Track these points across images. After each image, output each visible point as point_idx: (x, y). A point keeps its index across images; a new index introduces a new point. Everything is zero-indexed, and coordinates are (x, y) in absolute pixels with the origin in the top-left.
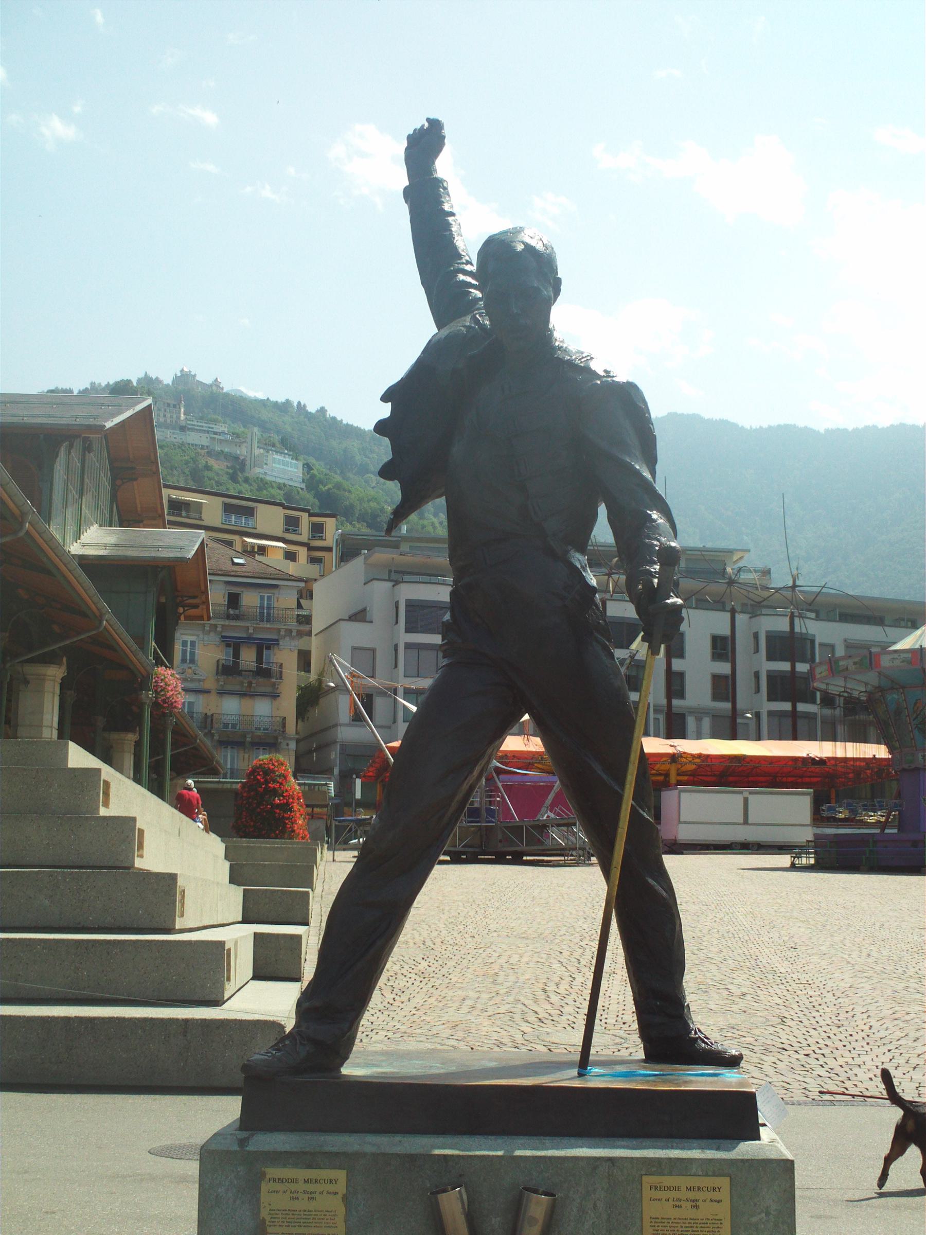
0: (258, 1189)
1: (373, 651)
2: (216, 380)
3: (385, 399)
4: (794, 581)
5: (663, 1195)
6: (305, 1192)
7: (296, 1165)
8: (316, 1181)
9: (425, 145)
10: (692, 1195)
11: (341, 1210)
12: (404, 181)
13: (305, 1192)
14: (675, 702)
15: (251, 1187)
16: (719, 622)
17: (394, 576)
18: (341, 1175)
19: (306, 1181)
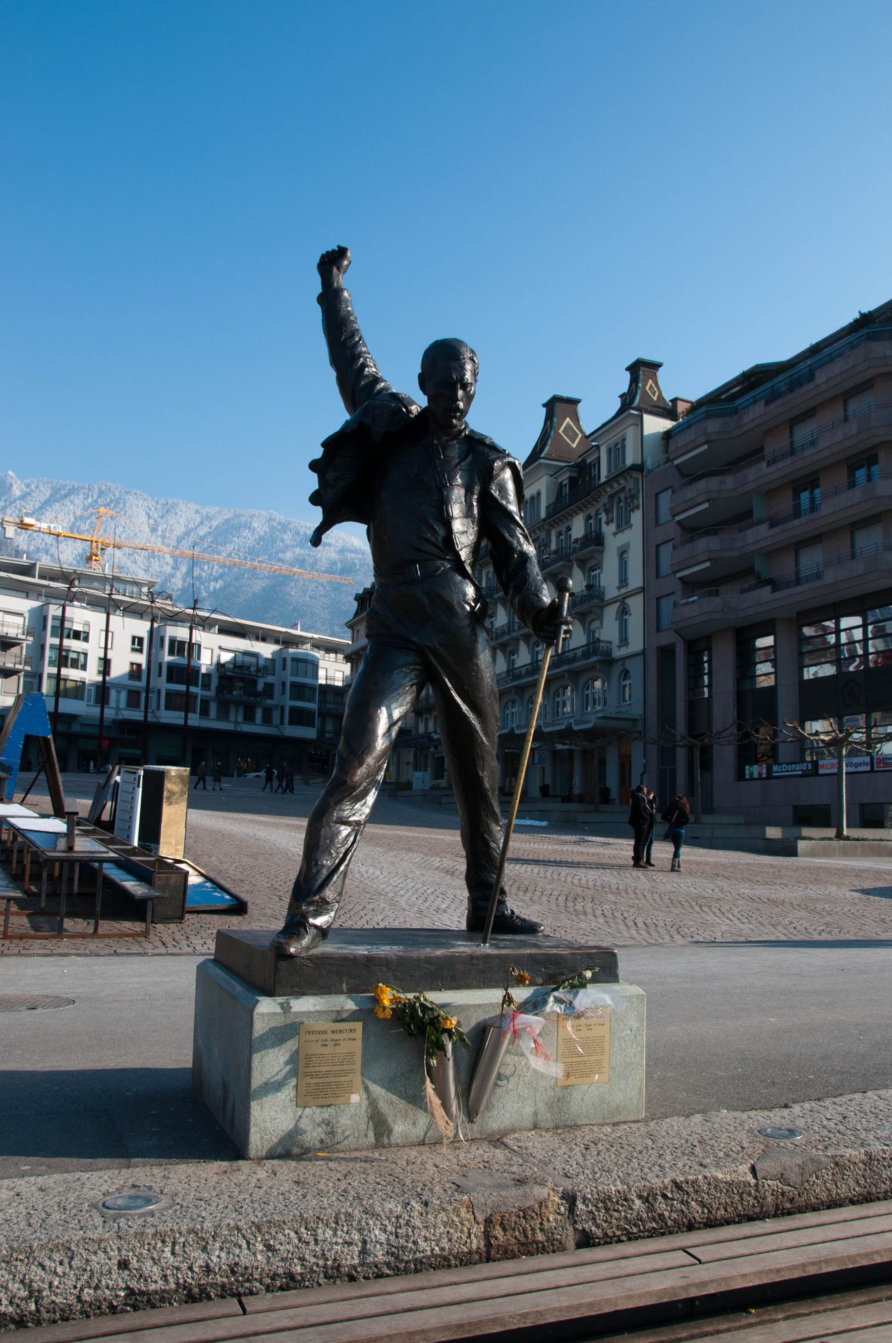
3: (323, 445)
6: (332, 1040)
8: (340, 1031)
9: (331, 261)
12: (319, 290)
13: (332, 1040)
19: (333, 1032)
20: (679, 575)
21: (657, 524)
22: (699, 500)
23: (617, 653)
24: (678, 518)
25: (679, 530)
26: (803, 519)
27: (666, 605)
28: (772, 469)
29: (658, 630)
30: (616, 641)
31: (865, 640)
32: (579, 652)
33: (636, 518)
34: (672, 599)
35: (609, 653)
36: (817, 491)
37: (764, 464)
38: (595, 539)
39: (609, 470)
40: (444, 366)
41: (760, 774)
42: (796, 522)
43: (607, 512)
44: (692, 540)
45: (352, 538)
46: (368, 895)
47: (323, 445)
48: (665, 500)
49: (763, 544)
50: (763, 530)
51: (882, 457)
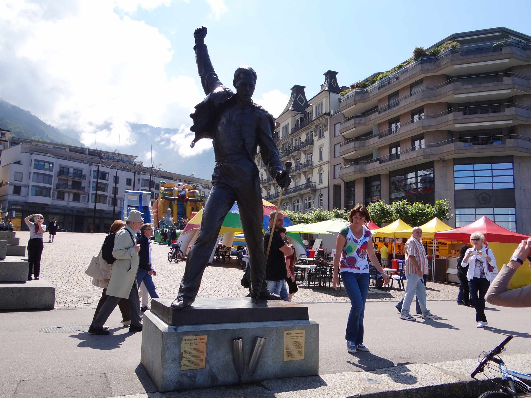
0: (181, 343)
1: (22, 173)
2: (338, 73)
3: (195, 108)
5: (289, 336)
7: (192, 335)
9: (200, 34)
10: (296, 335)
11: (205, 347)
15: (179, 343)
16: (130, 175)
17: (31, 152)
18: (205, 337)
20: (342, 157)
21: (334, 136)
22: (351, 127)
23: (318, 187)
24: (342, 134)
25: (343, 138)
26: (392, 135)
27: (338, 168)
28: (381, 115)
29: (334, 178)
30: (318, 182)
31: (417, 183)
32: (303, 187)
33: (326, 134)
34: (340, 166)
35: (315, 187)
36: (398, 124)
37: (378, 113)
38: (310, 142)
39: (316, 115)
40: (246, 79)
42: (390, 136)
43: (315, 131)
44: (348, 143)
45: (207, 144)
46: (218, 282)
47: (195, 108)
48: (338, 127)
49: (376, 144)
50: (376, 139)
51: (425, 111)
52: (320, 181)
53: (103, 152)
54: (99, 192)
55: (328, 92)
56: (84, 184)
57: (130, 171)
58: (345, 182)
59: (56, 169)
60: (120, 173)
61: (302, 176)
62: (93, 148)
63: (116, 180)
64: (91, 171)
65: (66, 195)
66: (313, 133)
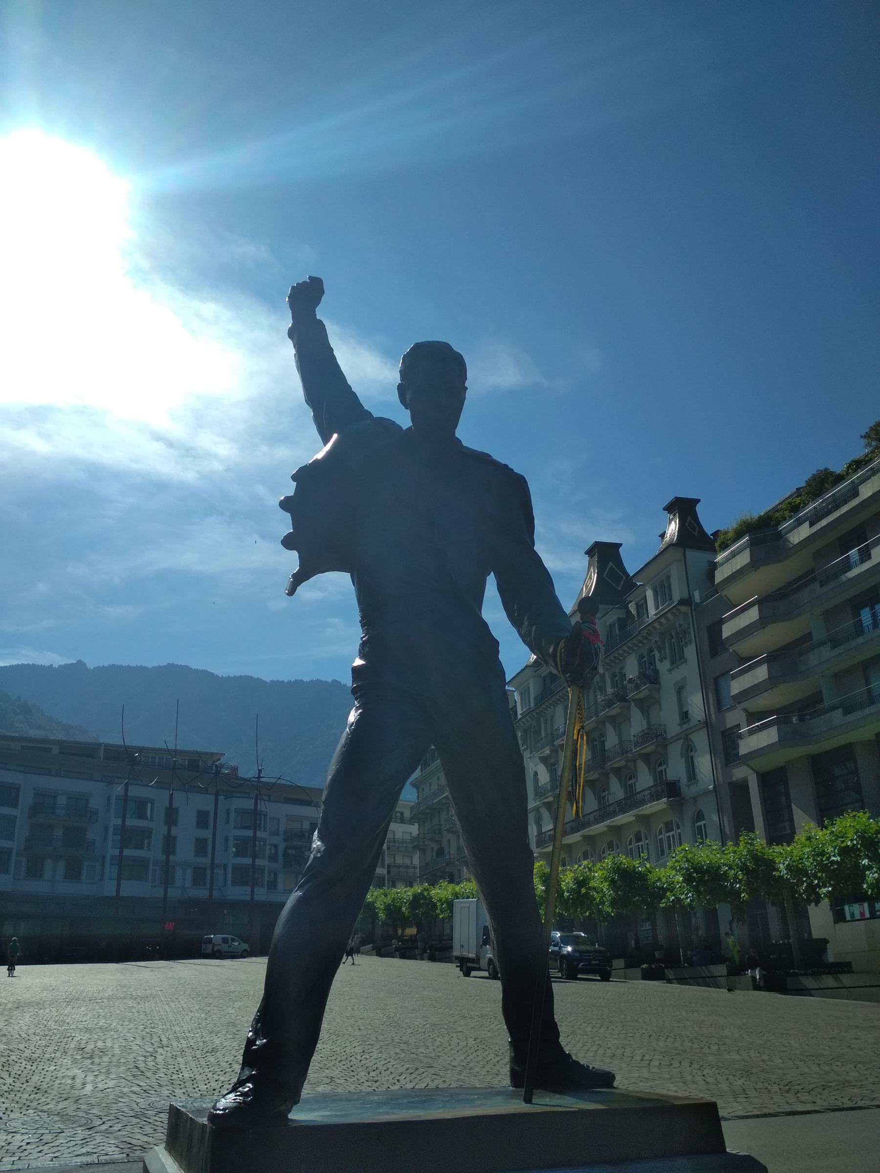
2: (699, 501)
3: (294, 478)
4: (260, 771)
14: (172, 858)
16: (205, 802)
30: (684, 780)
33: (690, 652)
37: (817, 584)
41: (862, 914)
42: (860, 640)
43: (660, 650)
45: (336, 585)
47: (294, 478)
52: (688, 772)
53: (141, 750)
54: (127, 852)
55: (681, 549)
56: (93, 834)
57: (205, 791)
58: (757, 773)
59: (26, 799)
60: (180, 799)
61: (636, 715)
62: (114, 739)
63: (171, 817)
64: (109, 799)
65: (49, 865)
66: (656, 654)
